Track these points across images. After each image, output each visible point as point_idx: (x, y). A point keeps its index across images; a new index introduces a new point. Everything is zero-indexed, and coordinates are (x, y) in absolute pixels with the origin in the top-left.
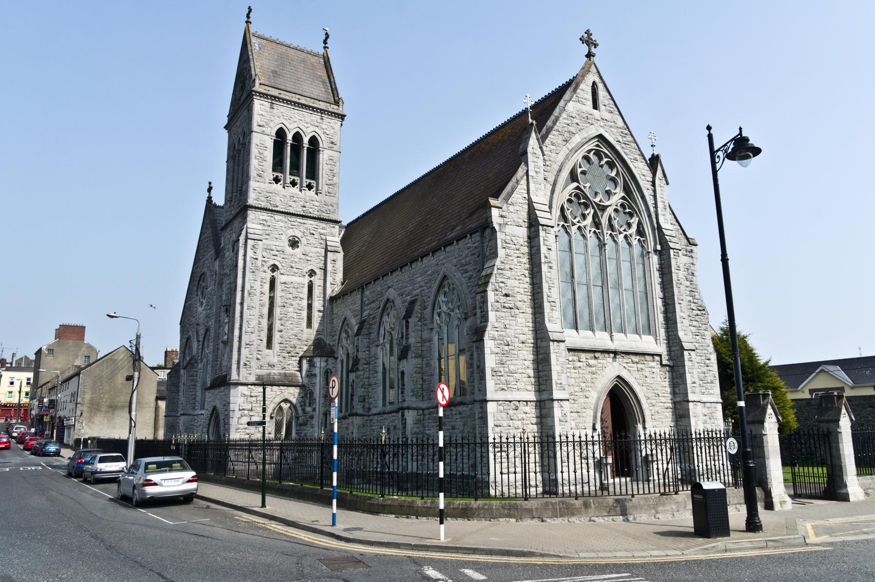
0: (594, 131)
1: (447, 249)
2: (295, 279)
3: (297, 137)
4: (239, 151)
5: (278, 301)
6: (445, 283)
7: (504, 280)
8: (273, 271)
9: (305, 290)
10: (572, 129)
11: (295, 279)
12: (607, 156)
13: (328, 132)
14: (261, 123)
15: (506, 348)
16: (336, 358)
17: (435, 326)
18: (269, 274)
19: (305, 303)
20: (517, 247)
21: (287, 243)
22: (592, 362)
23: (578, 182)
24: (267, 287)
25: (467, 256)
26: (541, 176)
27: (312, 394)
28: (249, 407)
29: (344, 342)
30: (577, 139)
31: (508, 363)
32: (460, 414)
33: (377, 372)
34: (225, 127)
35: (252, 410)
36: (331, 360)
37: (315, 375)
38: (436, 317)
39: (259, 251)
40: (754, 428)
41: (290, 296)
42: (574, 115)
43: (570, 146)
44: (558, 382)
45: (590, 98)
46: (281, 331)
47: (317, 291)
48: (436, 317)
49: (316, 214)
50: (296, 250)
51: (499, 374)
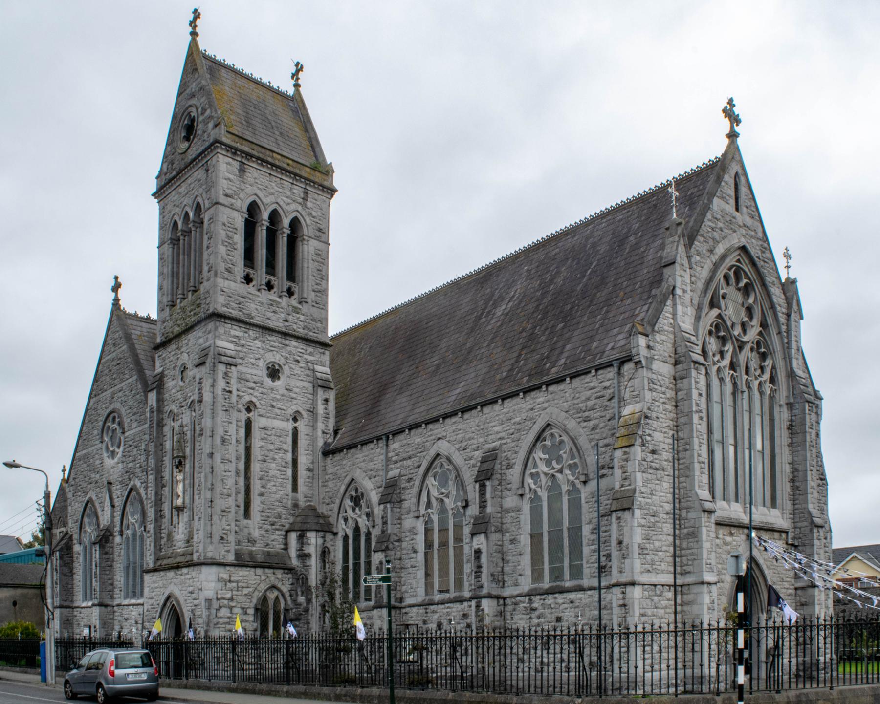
0: (736, 240)
1: (551, 388)
2: (277, 423)
3: (274, 216)
4: (187, 233)
5: (256, 453)
6: (547, 433)
7: (651, 432)
8: (249, 410)
9: (289, 440)
10: (716, 235)
11: (277, 423)
12: (747, 277)
13: (314, 214)
14: (229, 192)
15: (652, 519)
16: (335, 534)
17: (527, 491)
18: (244, 416)
19: (289, 457)
20: (664, 389)
21: (265, 372)
22: (728, 539)
23: (720, 308)
24: (242, 432)
25: (588, 399)
26: (688, 297)
27: (305, 580)
28: (229, 595)
29: (350, 513)
30: (720, 250)
31: (654, 538)
32: (572, 602)
33: (415, 552)
34: (154, 195)
35: (231, 599)
36: (329, 536)
37: (308, 556)
38: (529, 480)
39: (233, 381)
40: (24, 662)
41: (272, 447)
42: (719, 217)
43: (715, 258)
44: (709, 561)
45: (733, 194)
46: (262, 495)
47: (302, 442)
48: (529, 480)
49: (302, 332)
50: (277, 383)
51: (646, 552)
